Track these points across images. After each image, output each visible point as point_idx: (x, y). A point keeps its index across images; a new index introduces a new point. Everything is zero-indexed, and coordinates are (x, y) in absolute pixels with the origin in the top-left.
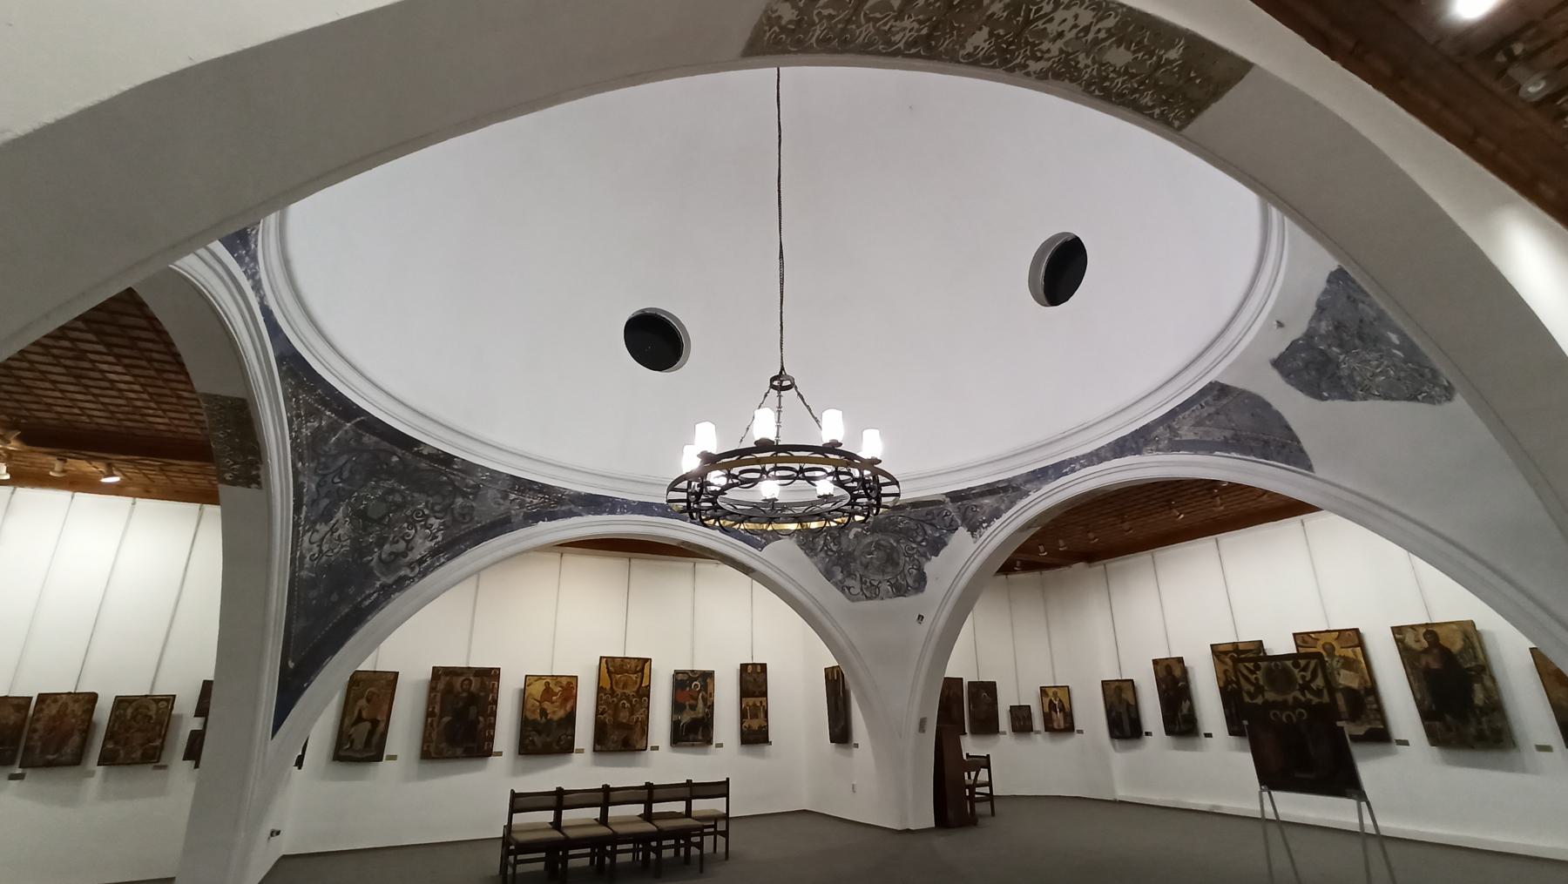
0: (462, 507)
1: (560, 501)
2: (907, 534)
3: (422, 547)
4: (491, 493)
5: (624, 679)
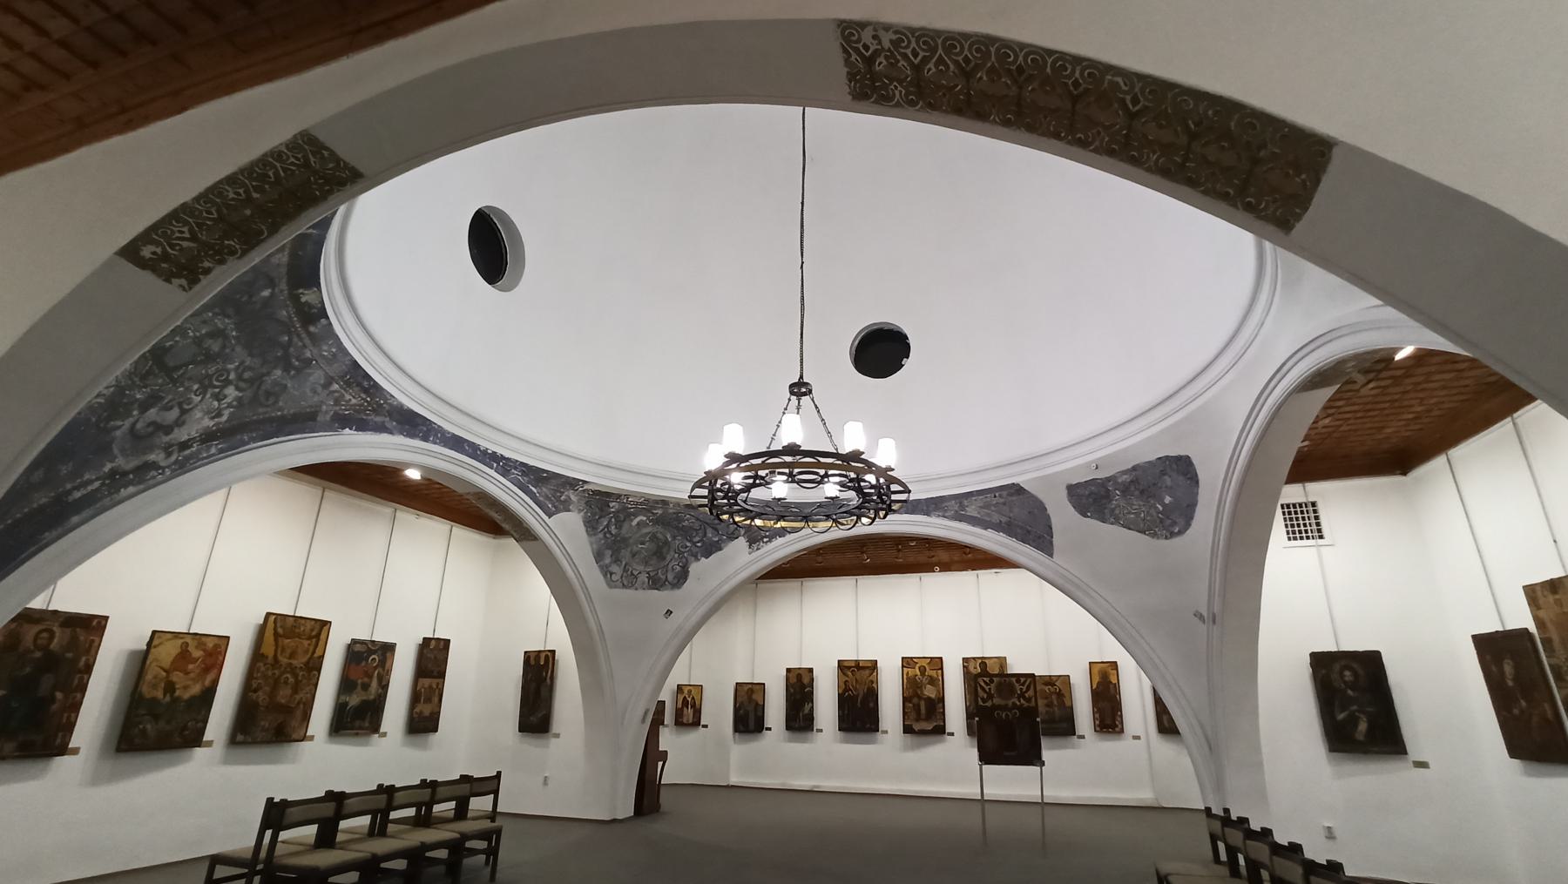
0: (276, 383)
1: (378, 409)
2: (686, 533)
3: (200, 422)
4: (317, 376)
5: (289, 644)
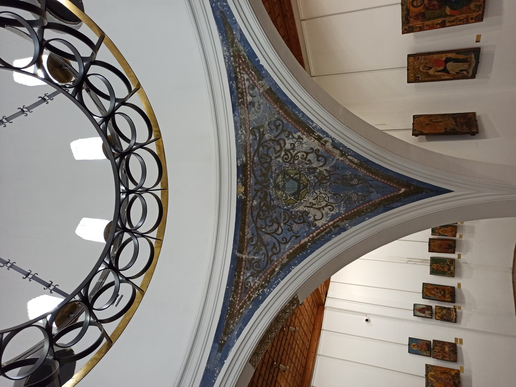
1: (237, 55)
3: (309, 142)
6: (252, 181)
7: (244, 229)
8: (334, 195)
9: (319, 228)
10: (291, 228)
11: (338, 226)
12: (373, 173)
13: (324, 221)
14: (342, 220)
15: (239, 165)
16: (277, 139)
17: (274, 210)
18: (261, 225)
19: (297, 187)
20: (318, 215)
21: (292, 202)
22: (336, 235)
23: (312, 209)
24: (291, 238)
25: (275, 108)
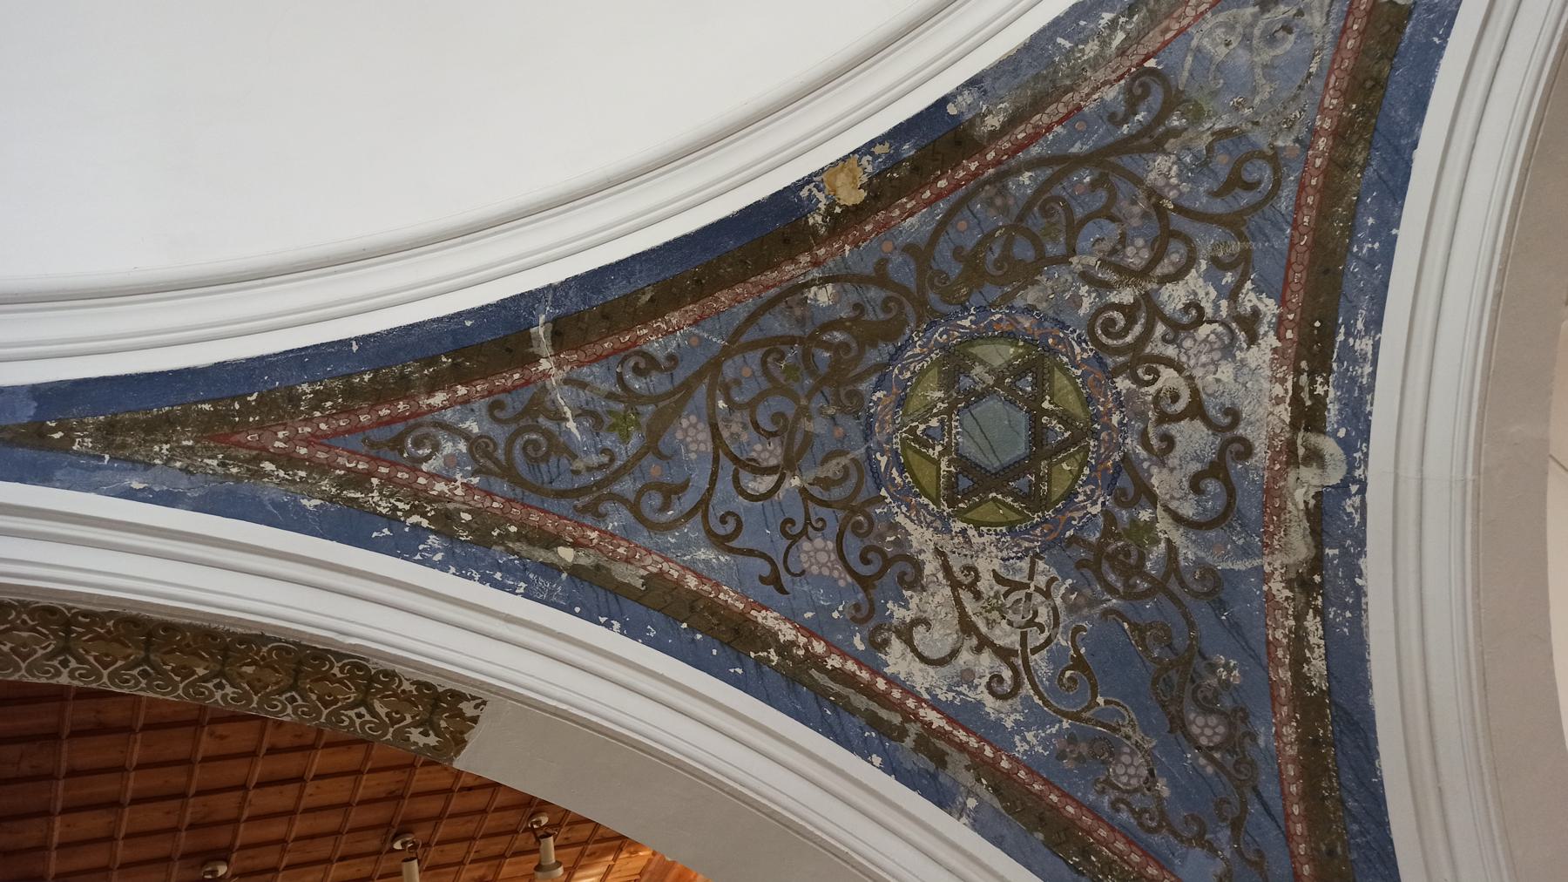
3: (1256, 383)
6: (914, 223)
7: (676, 304)
8: (1079, 663)
9: (876, 672)
10: (804, 532)
11: (940, 759)
12: (1312, 795)
13: (924, 679)
14: (981, 767)
15: (952, 109)
16: (1179, 222)
17: (843, 410)
18: (737, 382)
19: (1007, 459)
20: (936, 640)
21: (926, 475)
22: (890, 768)
23: (948, 591)
24: (750, 553)
25: (1321, 109)
